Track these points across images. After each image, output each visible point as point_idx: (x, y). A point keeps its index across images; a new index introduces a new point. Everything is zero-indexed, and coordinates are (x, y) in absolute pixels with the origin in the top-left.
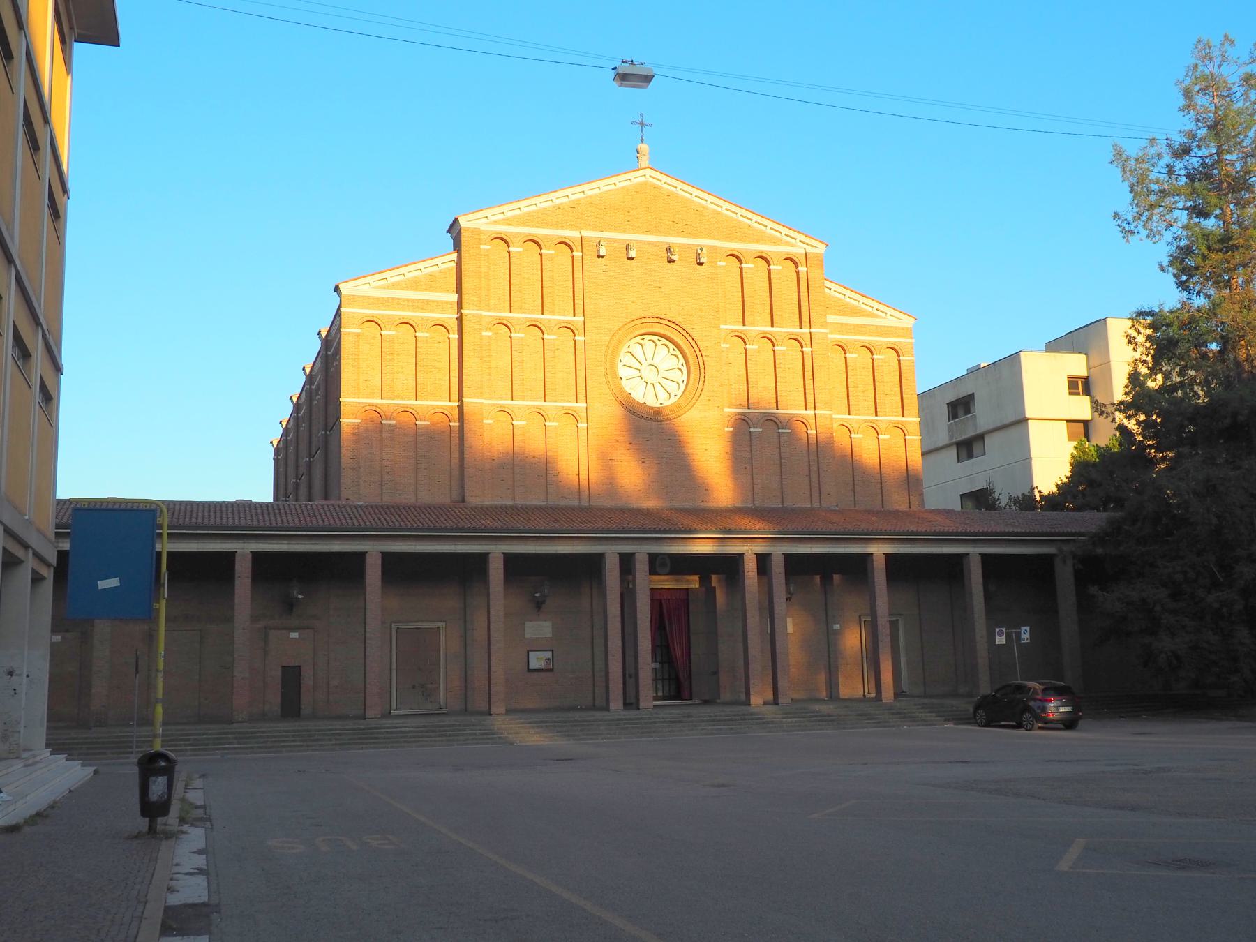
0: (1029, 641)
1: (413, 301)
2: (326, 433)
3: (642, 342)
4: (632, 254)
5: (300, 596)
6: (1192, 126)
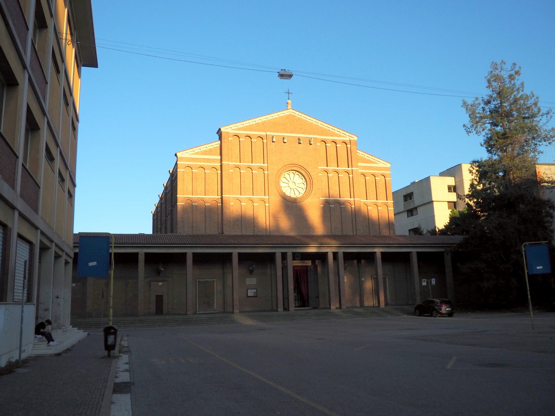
0: (435, 284)
1: (204, 159)
3: (289, 173)
4: (285, 141)
6: (491, 93)
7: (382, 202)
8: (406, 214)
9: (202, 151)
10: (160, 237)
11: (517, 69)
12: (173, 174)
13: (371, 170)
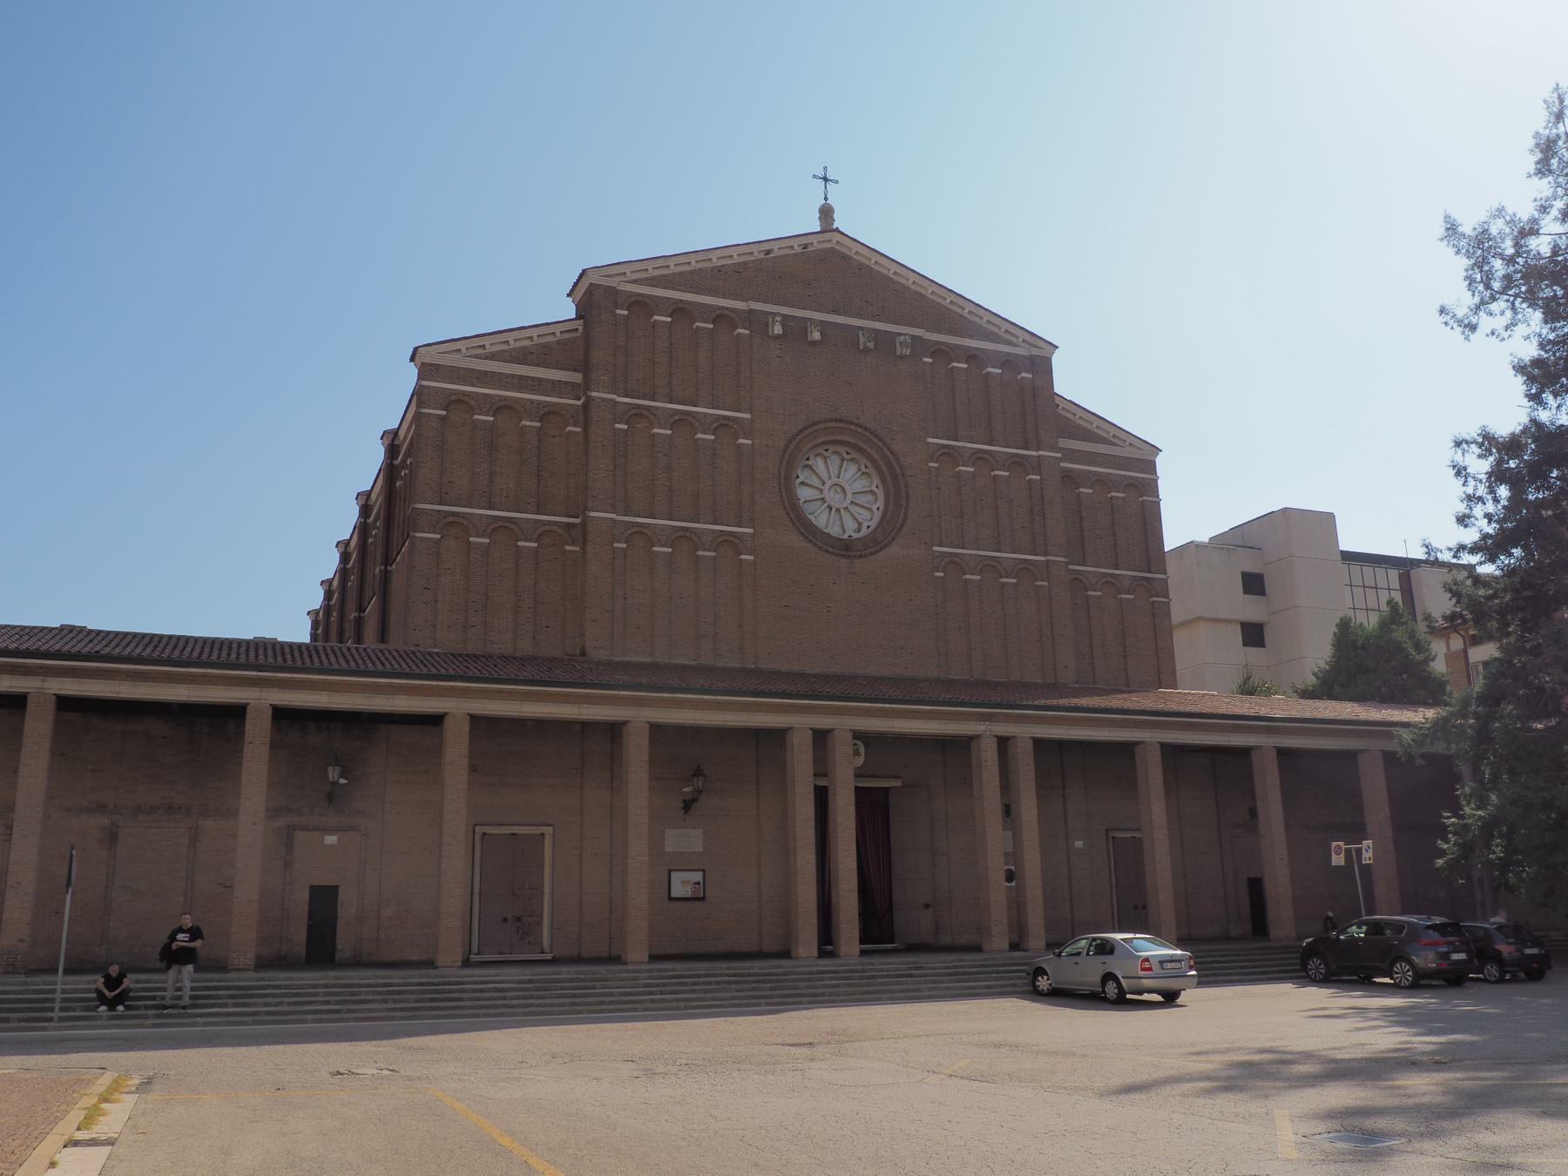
2: (386, 568)
5: (343, 781)
9: (514, 349)
12: (398, 446)
13: (1100, 466)
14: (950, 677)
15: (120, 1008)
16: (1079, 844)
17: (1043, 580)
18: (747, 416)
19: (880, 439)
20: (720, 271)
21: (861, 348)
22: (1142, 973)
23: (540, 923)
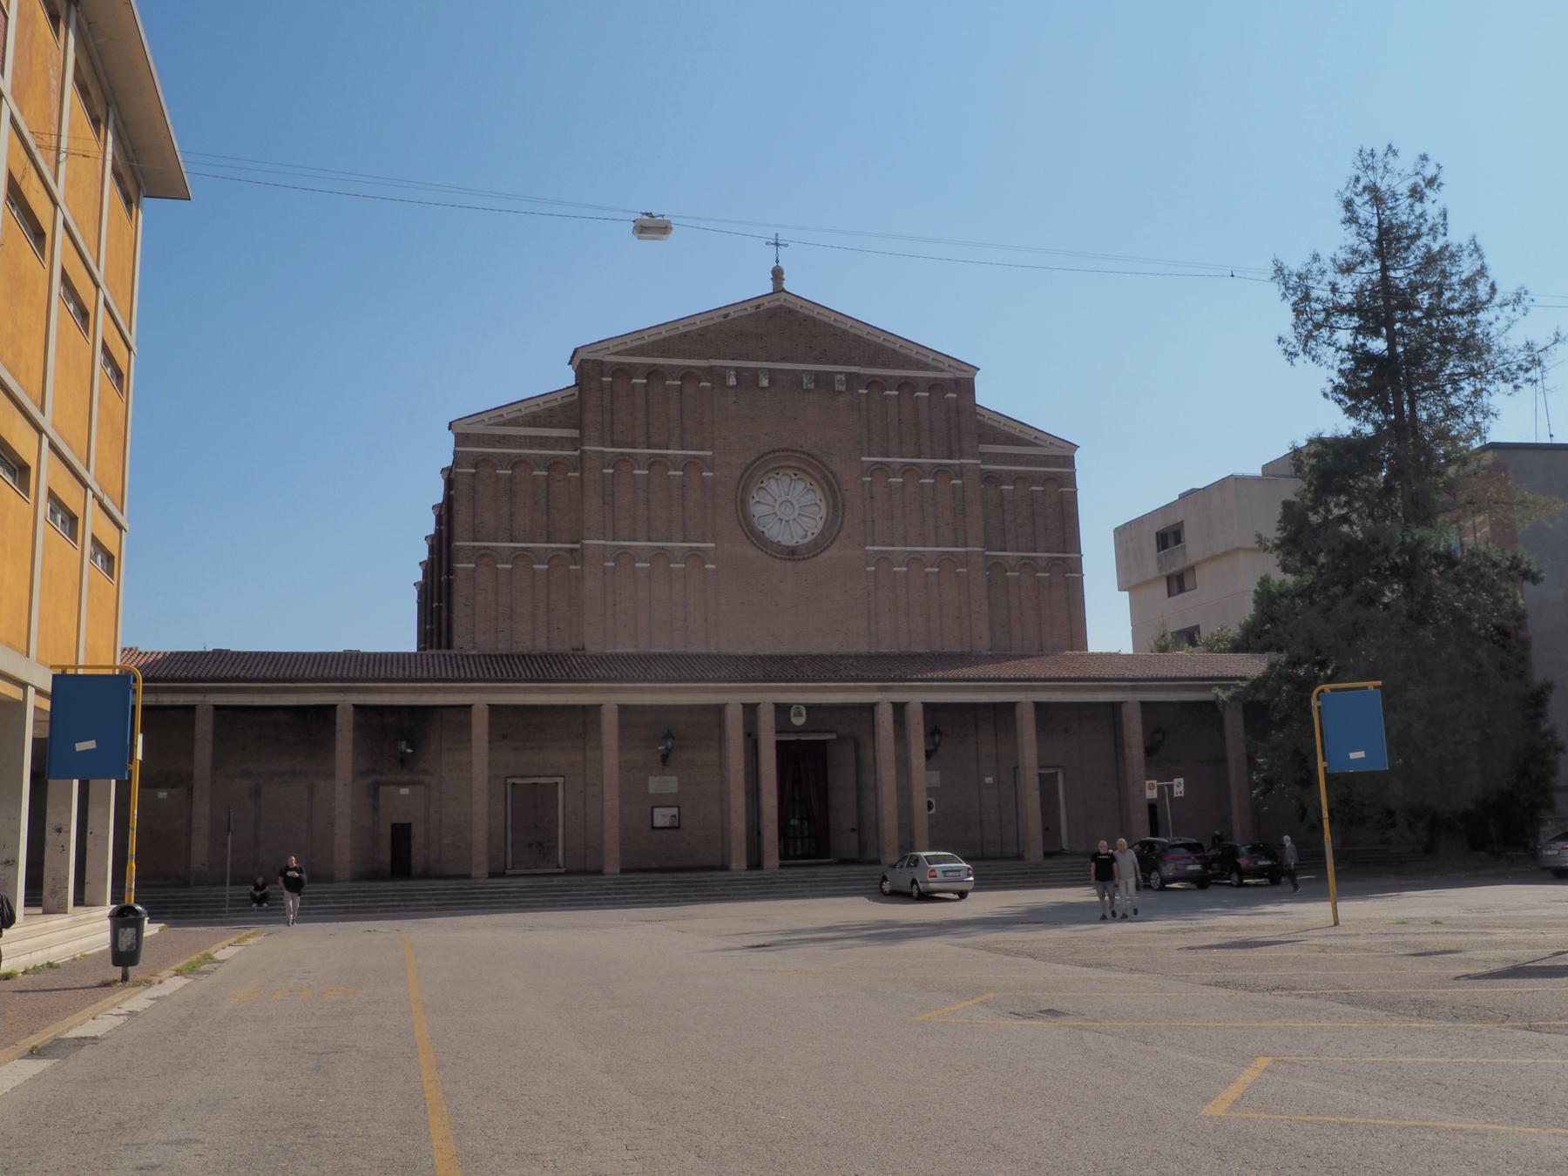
0: (1182, 795)
5: (409, 751)
6: (1354, 241)
7: (1051, 558)
8: (1163, 587)
9: (526, 415)
10: (401, 662)
11: (1430, 171)
14: (880, 650)
15: (265, 905)
16: (989, 780)
17: (963, 567)
18: (710, 453)
19: (821, 462)
20: (686, 336)
21: (805, 387)
22: (930, 879)
23: (556, 847)
